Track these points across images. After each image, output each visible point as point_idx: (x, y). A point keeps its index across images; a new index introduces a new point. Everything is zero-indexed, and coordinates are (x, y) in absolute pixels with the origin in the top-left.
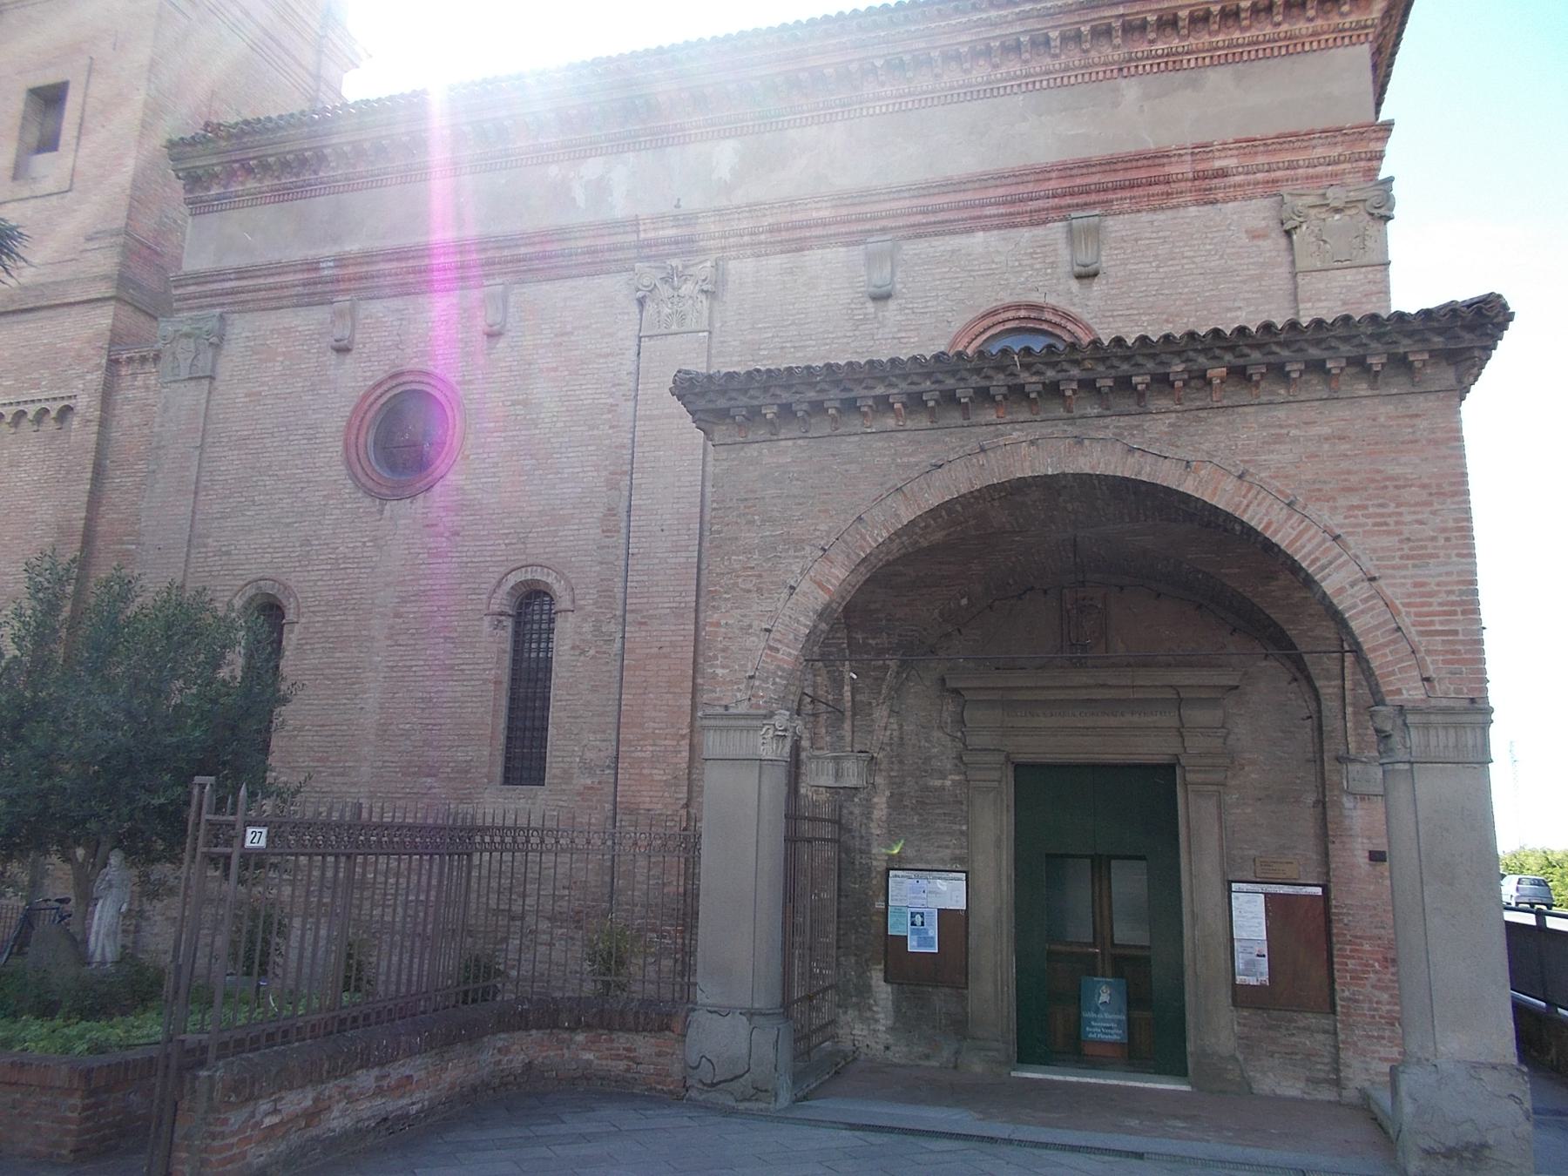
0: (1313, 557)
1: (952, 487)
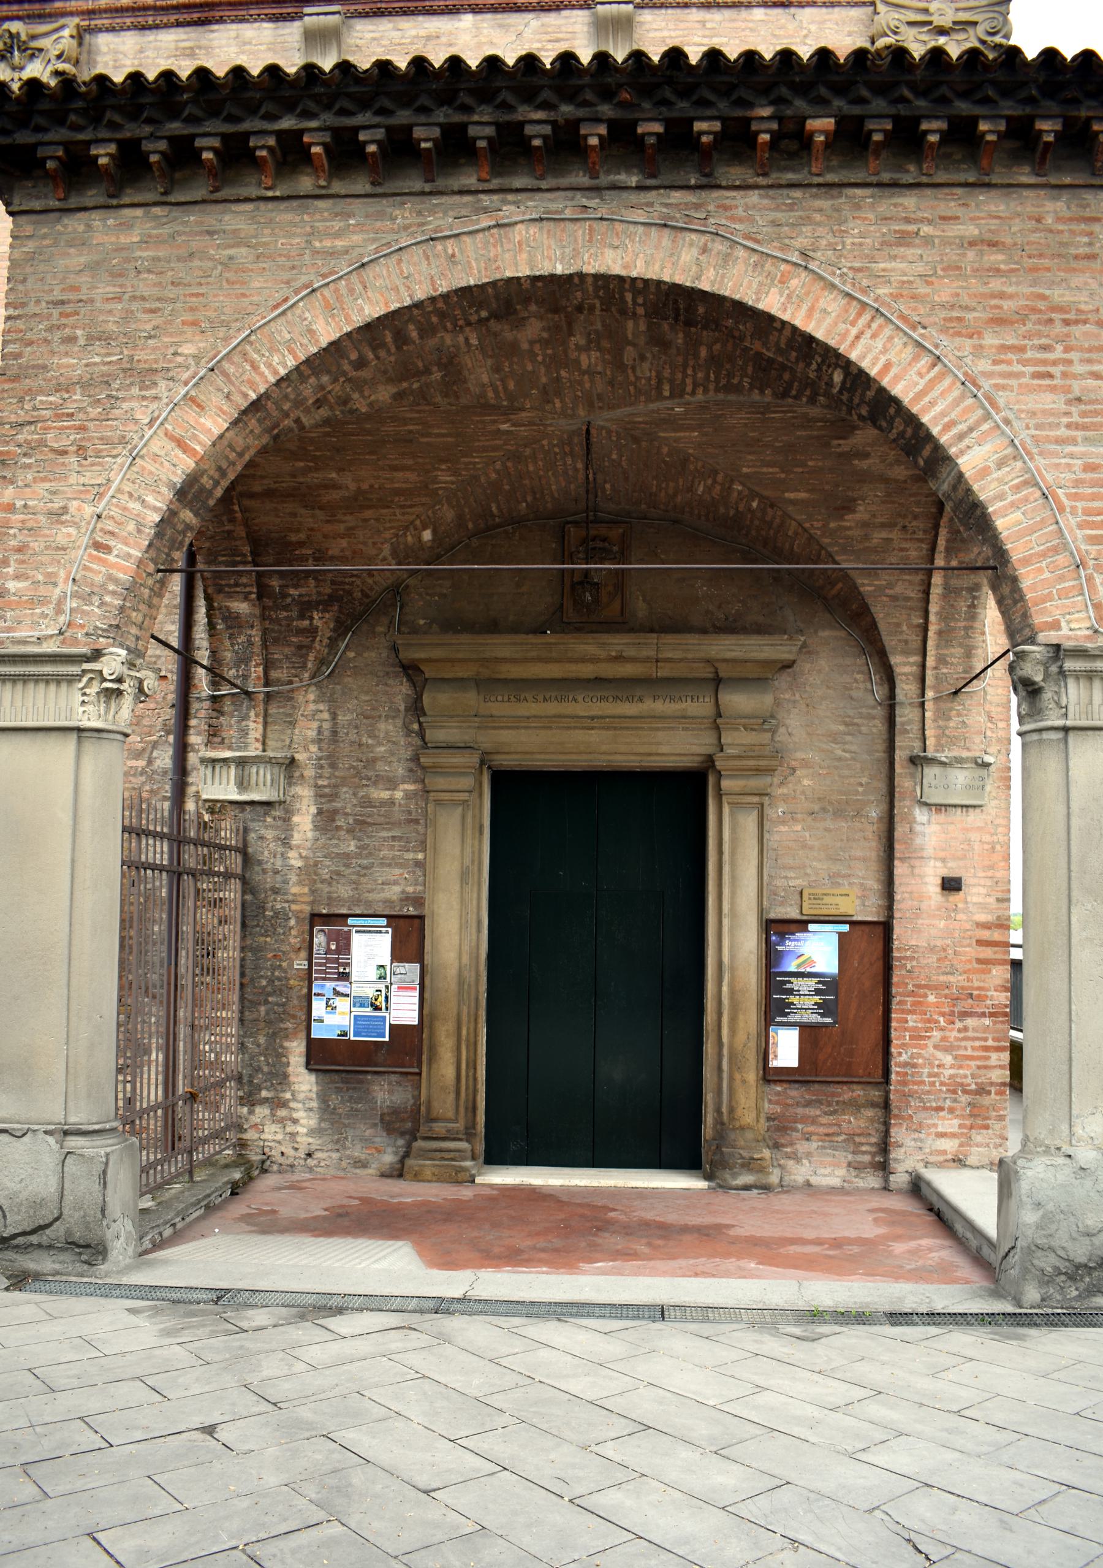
0: (946, 420)
1: (402, 289)
